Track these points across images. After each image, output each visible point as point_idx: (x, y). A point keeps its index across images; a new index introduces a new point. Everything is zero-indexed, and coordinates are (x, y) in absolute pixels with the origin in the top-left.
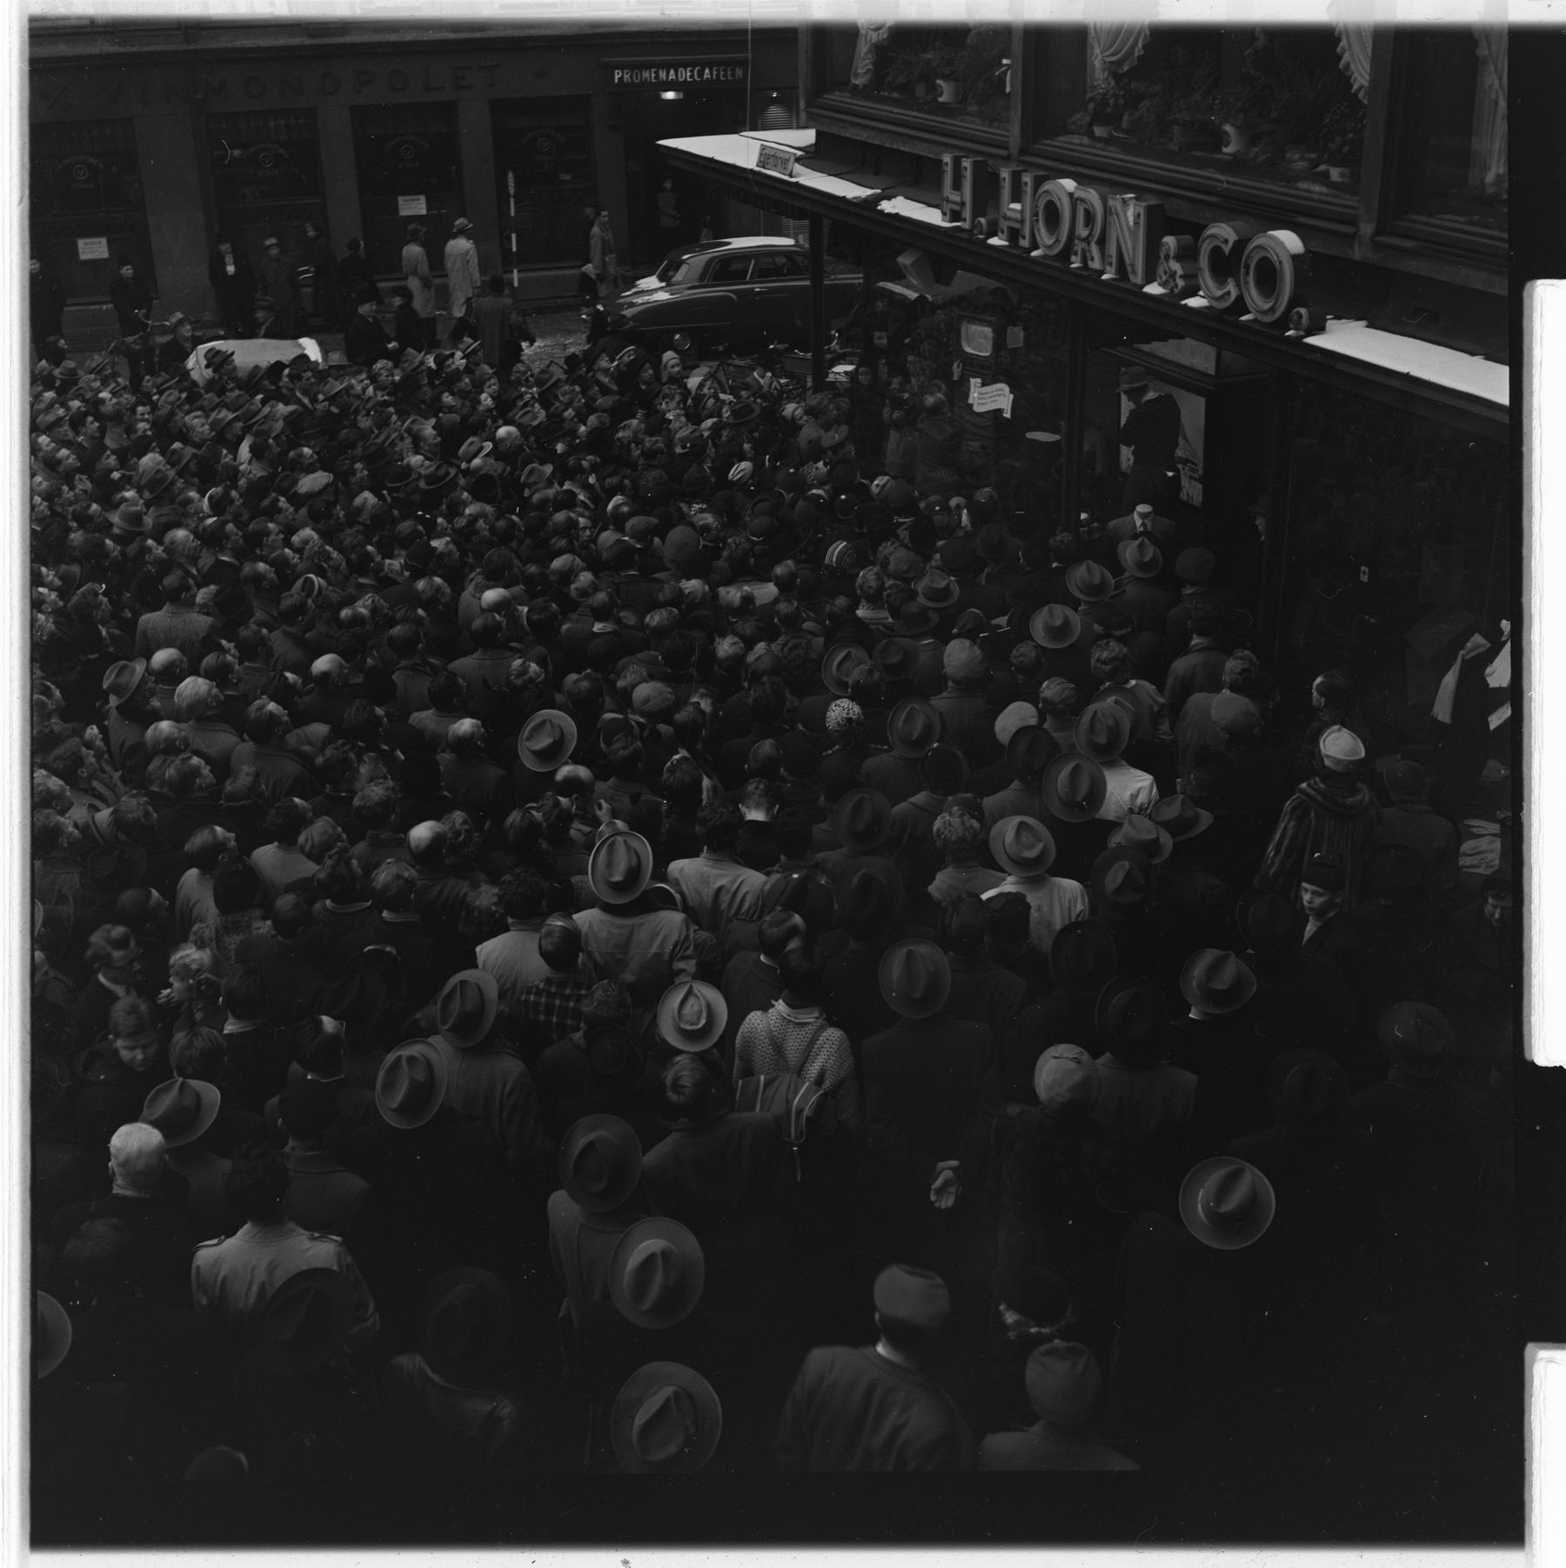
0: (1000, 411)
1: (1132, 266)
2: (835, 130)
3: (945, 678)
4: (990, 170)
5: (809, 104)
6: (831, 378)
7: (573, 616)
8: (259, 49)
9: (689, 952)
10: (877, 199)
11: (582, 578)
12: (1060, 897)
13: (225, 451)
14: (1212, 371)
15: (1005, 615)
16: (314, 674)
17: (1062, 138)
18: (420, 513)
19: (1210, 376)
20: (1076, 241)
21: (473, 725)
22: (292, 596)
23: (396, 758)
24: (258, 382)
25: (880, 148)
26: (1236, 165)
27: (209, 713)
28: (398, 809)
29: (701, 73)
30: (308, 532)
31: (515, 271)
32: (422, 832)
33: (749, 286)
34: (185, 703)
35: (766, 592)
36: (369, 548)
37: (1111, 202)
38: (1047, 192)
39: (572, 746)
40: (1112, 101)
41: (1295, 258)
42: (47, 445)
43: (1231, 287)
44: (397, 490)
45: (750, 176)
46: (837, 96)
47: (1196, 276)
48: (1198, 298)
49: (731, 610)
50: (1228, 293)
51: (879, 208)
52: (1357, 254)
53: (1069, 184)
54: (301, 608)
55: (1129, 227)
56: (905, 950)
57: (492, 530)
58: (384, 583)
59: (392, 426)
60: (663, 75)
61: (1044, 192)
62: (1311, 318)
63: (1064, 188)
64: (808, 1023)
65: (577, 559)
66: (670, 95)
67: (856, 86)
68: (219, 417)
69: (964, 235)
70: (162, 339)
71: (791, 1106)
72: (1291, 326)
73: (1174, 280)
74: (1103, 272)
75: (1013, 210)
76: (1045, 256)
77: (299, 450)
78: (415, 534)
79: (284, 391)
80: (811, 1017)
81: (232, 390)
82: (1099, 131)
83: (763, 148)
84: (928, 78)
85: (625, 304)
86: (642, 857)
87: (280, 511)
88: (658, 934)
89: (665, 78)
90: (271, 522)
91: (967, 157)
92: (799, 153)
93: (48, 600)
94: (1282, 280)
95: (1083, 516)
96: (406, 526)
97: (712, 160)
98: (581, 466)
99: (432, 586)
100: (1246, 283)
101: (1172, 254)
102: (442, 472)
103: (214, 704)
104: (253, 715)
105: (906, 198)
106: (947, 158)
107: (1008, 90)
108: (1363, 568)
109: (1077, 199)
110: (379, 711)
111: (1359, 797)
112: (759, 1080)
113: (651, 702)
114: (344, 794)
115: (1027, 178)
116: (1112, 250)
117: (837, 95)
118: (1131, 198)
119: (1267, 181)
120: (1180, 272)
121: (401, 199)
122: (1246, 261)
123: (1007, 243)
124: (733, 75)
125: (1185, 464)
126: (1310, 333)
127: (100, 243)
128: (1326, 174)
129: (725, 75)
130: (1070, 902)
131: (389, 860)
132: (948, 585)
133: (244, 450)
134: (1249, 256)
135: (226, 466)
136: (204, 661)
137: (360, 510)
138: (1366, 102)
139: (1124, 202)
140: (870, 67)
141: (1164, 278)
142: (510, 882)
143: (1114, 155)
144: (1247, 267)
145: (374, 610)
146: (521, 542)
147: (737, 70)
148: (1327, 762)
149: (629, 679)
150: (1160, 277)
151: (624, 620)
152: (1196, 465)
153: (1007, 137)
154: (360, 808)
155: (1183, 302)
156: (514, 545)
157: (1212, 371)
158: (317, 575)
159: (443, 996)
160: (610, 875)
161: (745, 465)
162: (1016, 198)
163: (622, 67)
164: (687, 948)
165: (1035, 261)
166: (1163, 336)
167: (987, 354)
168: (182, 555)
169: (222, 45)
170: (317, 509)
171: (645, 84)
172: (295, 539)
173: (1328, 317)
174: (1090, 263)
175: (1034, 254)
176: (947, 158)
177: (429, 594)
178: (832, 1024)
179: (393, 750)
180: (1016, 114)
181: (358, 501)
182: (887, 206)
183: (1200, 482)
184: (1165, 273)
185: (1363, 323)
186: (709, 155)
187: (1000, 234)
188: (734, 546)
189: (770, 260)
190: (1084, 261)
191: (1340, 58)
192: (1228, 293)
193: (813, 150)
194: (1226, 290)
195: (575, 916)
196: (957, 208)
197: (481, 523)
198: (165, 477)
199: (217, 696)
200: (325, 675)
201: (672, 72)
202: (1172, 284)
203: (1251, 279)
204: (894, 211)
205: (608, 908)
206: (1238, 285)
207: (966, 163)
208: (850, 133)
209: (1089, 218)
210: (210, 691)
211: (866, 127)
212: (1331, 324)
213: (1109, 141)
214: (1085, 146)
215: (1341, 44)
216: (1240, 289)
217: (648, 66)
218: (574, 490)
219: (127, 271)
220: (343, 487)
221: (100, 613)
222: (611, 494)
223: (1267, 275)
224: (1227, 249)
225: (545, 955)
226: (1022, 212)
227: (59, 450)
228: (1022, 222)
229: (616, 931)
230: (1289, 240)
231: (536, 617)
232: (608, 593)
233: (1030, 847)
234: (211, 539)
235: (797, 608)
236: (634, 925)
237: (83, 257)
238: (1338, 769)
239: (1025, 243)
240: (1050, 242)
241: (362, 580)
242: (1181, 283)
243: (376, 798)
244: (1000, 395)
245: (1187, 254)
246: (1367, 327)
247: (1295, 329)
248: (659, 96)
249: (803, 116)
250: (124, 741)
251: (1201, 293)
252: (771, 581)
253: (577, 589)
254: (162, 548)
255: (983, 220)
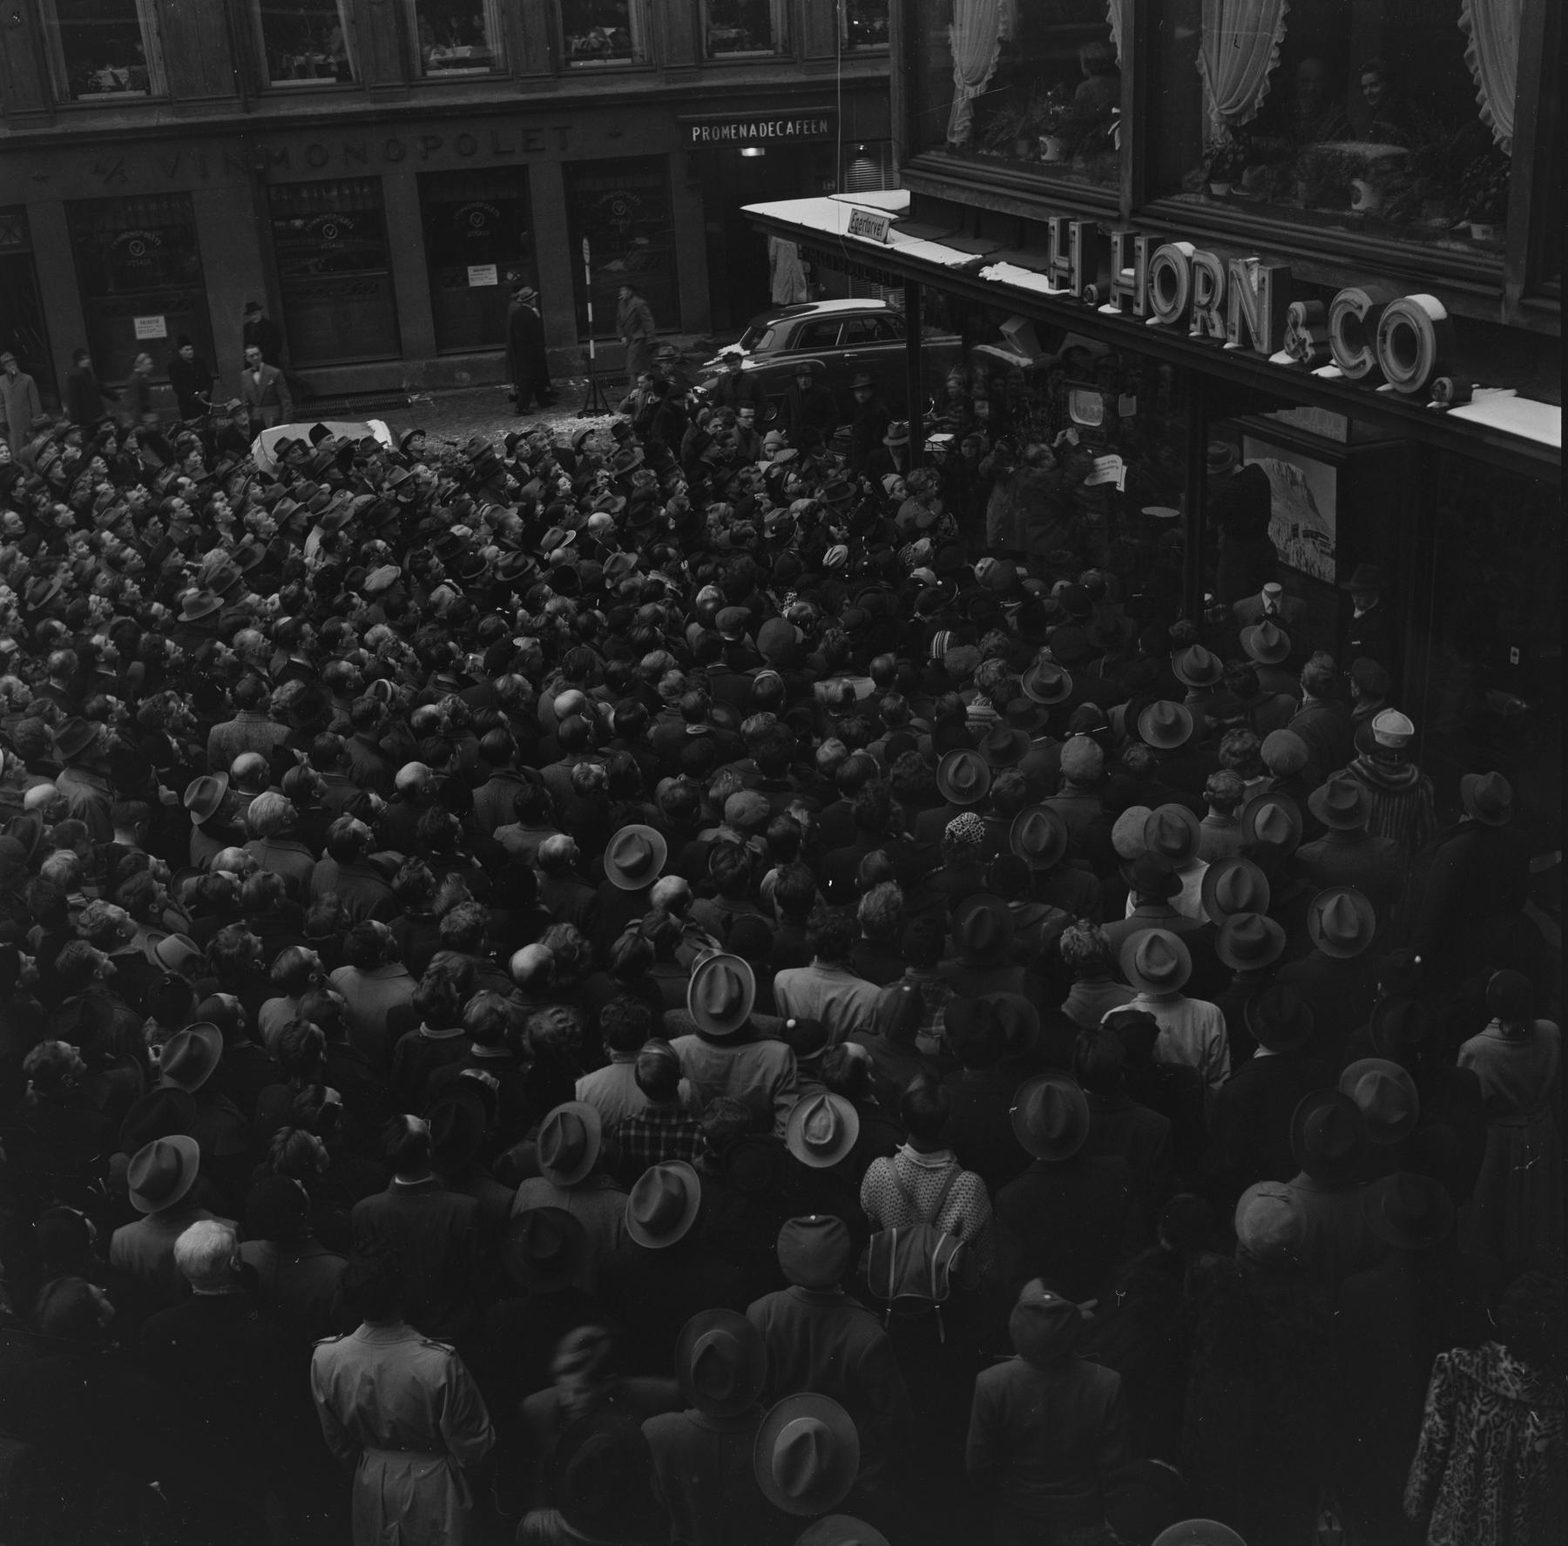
0: (1114, 484)
1: (1258, 334)
2: (931, 192)
3: (1062, 775)
4: (1099, 232)
5: (904, 165)
6: (928, 448)
7: (660, 716)
8: (322, 117)
9: (792, 1086)
10: (978, 266)
11: (671, 675)
12: (1193, 1020)
13: (292, 546)
14: (1343, 438)
15: (1123, 702)
16: (399, 787)
17: (1177, 198)
18: (499, 609)
19: (1342, 444)
20: (1195, 309)
21: (566, 843)
22: (363, 700)
23: (472, 865)
24: (327, 469)
25: (979, 211)
26: (1365, 223)
27: (282, 832)
28: (486, 933)
29: (783, 128)
30: (382, 629)
31: (592, 342)
32: (524, 958)
33: (839, 352)
34: (259, 821)
35: (865, 687)
36: (451, 644)
37: (1232, 267)
38: (1162, 256)
39: (662, 860)
40: (1230, 157)
41: (1437, 324)
42: (112, 541)
43: (1366, 355)
44: (473, 581)
45: (841, 242)
46: (932, 156)
47: (1327, 344)
48: (1330, 367)
49: (832, 704)
50: (1364, 362)
51: (981, 275)
52: (1504, 318)
53: (1186, 248)
54: (373, 713)
55: (1253, 293)
56: (1043, 1086)
57: (573, 625)
58: (463, 683)
59: (471, 516)
60: (743, 131)
61: (1160, 256)
62: (1456, 387)
63: (1181, 252)
64: (941, 1168)
65: (670, 656)
66: (751, 152)
67: (953, 145)
68: (283, 507)
69: (1071, 303)
70: (224, 423)
71: (930, 1260)
72: (1434, 397)
73: (1304, 349)
74: (1225, 341)
75: (1125, 276)
76: (1161, 324)
77: (372, 543)
78: (500, 630)
79: (353, 479)
80: (942, 1161)
81: (297, 479)
82: (1217, 189)
83: (855, 212)
84: (1031, 135)
85: (707, 373)
86: (743, 982)
87: (353, 607)
88: (759, 1066)
89: (745, 134)
90: (345, 621)
91: (1075, 220)
92: (893, 216)
93: (115, 709)
94: (1422, 346)
95: (1207, 597)
96: (489, 622)
97: (801, 226)
98: (667, 553)
99: (512, 686)
100: (1383, 351)
101: (1300, 322)
102: (519, 563)
103: (289, 822)
104: (336, 835)
105: (1009, 263)
106: (1054, 222)
107: (1117, 146)
108: (1513, 649)
109: (1195, 264)
110: (454, 818)
111: (1406, 775)
112: (891, 1233)
113: (746, 814)
114: (426, 914)
115: (1141, 242)
116: (1235, 318)
117: (933, 155)
118: (1254, 262)
119: (1402, 240)
120: (1309, 340)
121: (471, 270)
122: (1383, 327)
123: (1120, 311)
124: (817, 128)
125: (1315, 538)
126: (1454, 404)
127: (157, 321)
128: (1467, 233)
129: (809, 129)
130: (1204, 1025)
131: (482, 992)
132: (1061, 678)
133: (313, 541)
134: (1386, 323)
135: (295, 560)
136: (286, 775)
137: (437, 605)
138: (1510, 154)
139: (1247, 266)
140: (968, 124)
141: (1293, 347)
142: (613, 1012)
143: (1235, 215)
144: (1384, 334)
145: (455, 713)
146: (603, 638)
147: (822, 123)
148: (1378, 738)
149: (721, 789)
150: (1288, 345)
151: (716, 718)
152: (1327, 539)
153: (1118, 197)
154: (447, 934)
155: (1314, 372)
156: (596, 641)
157: (1343, 438)
158: (389, 679)
159: (542, 1132)
160: (709, 1006)
161: (840, 549)
162: (1129, 262)
163: (700, 124)
164: (791, 1081)
165: (1151, 329)
166: (1291, 406)
167: (1096, 424)
168: (253, 656)
169: (283, 113)
170: (390, 604)
171: (725, 141)
172: (369, 636)
173: (1474, 386)
174: (1210, 331)
175: (1149, 322)
176: (1054, 222)
177: (509, 693)
178: (965, 1168)
179: (469, 857)
180: (1127, 175)
181: (435, 596)
182: (989, 273)
183: (1332, 557)
184: (1294, 341)
185: (1513, 392)
186: (797, 221)
187: (1112, 301)
188: (831, 639)
189: (860, 323)
190: (1205, 329)
191: (1480, 107)
192: (1364, 362)
193: (908, 212)
194: (1361, 359)
195: (672, 1042)
196: (1064, 274)
197: (560, 620)
198: (232, 575)
199: (292, 813)
200: (412, 786)
201: (753, 127)
202: (1302, 354)
203: (1388, 347)
204: (997, 278)
205: (705, 1037)
206: (1374, 353)
207: (1075, 227)
208: (949, 195)
209: (1209, 284)
210: (285, 807)
211: (964, 188)
212: (1478, 394)
213: (1228, 199)
214: (1202, 205)
215: (1480, 93)
216: (1376, 358)
217: (727, 122)
218: (661, 579)
219: (187, 351)
220: (418, 578)
221: (170, 721)
222: (703, 582)
223: (1406, 343)
224: (1361, 316)
225: (640, 1082)
226: (1136, 277)
227: (125, 548)
228: (1136, 288)
229: (715, 1061)
230: (1429, 305)
231: (624, 718)
232: (700, 694)
233: (1163, 964)
234: (283, 640)
235: (903, 705)
236: (734, 1056)
237: (140, 336)
238: (1387, 743)
239: (1139, 311)
240: (1166, 309)
241: (440, 678)
242: (1311, 352)
243: (464, 923)
244: (1112, 467)
245: (1316, 321)
246: (1516, 396)
247: (1439, 400)
248: (741, 153)
249: (897, 177)
250: (203, 859)
251: (1333, 362)
252: (869, 676)
253: (666, 687)
254: (232, 650)
255: (1093, 287)
